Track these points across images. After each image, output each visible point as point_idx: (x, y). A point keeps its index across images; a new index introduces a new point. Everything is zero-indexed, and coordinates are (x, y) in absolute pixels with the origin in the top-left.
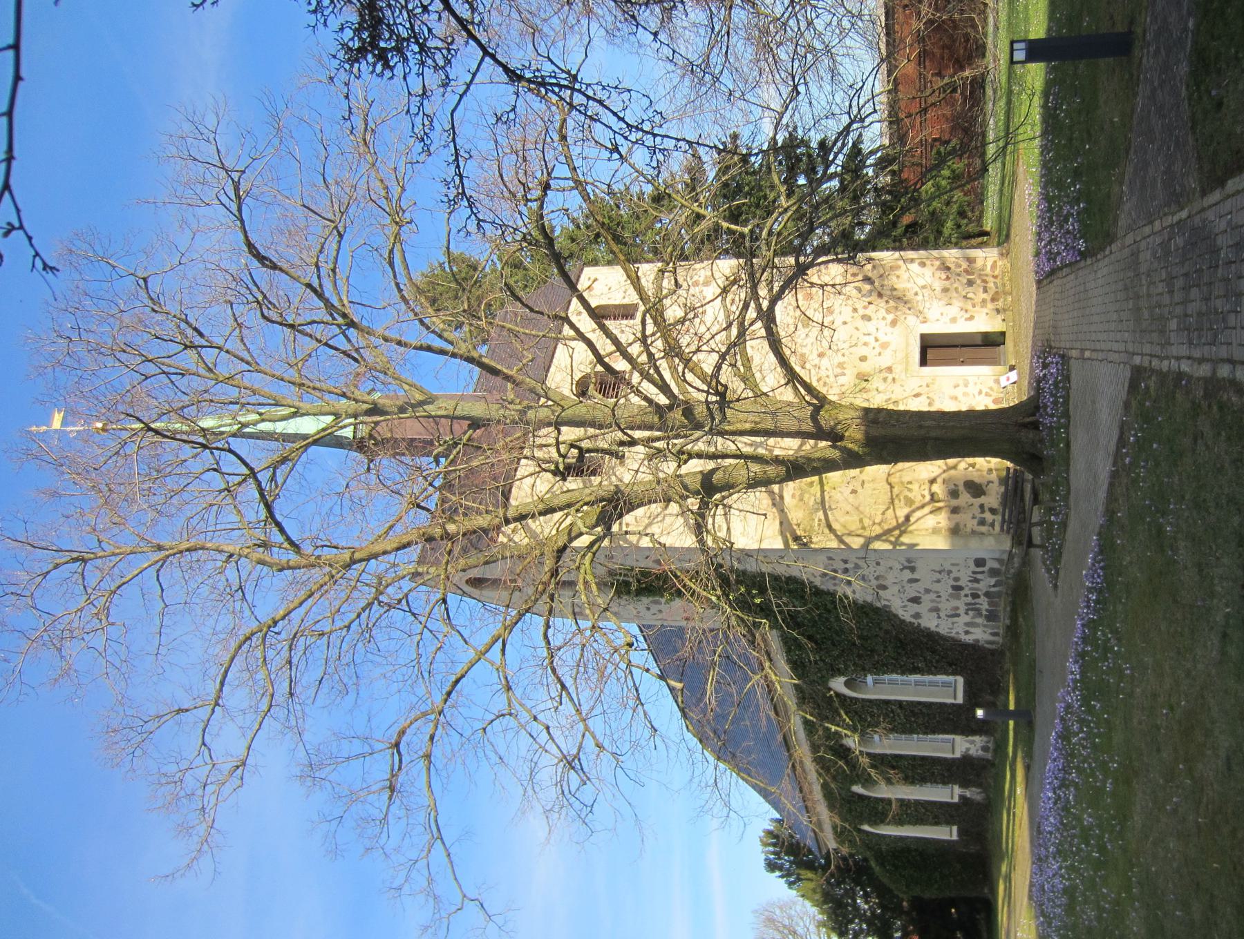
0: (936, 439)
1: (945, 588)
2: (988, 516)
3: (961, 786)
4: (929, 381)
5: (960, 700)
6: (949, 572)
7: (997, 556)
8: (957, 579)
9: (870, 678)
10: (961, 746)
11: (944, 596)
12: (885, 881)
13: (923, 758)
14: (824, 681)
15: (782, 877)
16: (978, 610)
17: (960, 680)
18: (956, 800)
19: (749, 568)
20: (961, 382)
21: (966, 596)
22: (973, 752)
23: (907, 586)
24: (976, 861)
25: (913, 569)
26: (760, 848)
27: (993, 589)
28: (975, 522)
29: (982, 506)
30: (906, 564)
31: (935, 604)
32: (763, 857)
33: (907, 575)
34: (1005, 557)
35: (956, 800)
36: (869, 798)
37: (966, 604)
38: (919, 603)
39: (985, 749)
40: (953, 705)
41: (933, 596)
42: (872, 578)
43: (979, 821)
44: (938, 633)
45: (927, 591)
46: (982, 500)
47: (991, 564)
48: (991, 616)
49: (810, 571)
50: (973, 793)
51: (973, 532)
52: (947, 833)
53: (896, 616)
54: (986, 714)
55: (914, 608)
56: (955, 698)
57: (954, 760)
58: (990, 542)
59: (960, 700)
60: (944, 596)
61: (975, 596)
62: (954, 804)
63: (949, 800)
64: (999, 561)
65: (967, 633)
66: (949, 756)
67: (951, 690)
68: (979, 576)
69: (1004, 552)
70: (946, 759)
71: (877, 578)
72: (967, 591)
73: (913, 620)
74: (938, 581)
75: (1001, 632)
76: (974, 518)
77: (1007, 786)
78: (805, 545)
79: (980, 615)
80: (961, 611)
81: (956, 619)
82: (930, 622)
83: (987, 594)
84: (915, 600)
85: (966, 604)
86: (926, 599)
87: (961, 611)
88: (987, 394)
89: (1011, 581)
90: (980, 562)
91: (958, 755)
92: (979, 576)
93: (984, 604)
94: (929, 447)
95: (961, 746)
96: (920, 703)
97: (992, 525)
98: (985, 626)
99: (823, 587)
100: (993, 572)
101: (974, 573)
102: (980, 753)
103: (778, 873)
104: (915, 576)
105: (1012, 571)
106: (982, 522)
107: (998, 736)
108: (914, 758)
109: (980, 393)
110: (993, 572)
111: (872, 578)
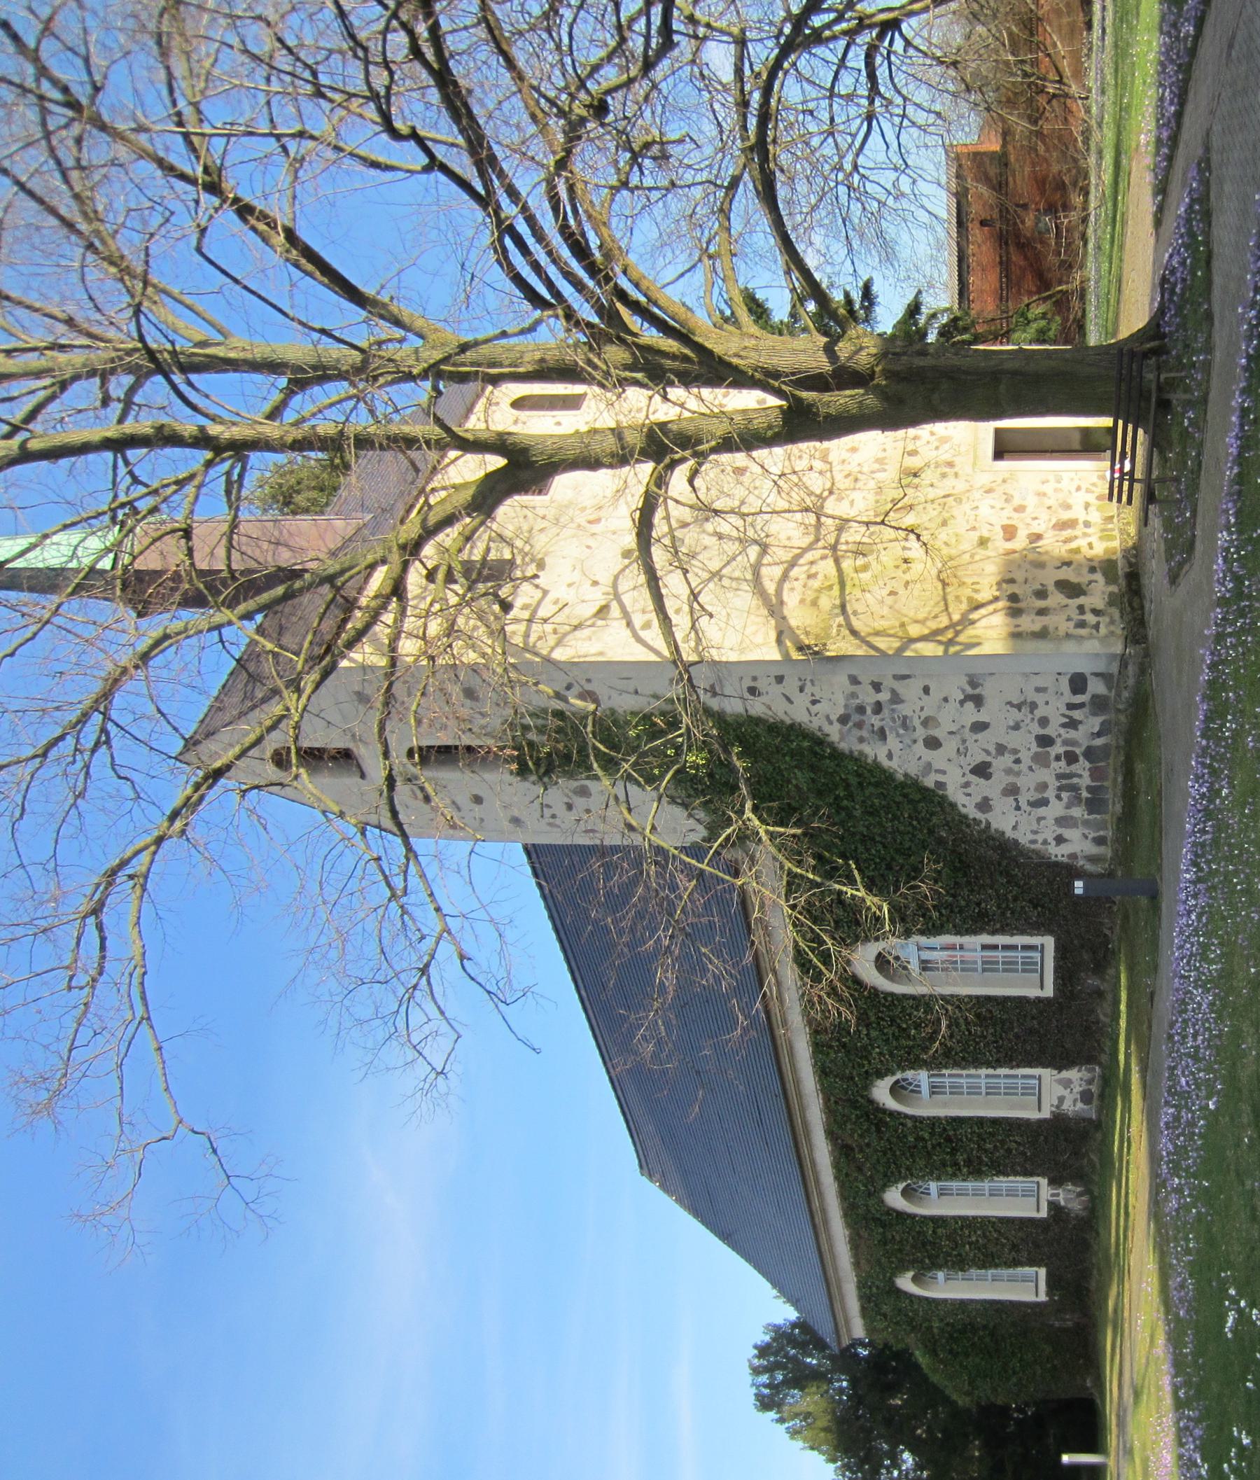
0: (1015, 373)
1: (1025, 743)
2: (1090, 618)
3: (1054, 1182)
4: (1007, 475)
5: (1049, 992)
6: (1033, 706)
7: (1101, 667)
8: (1044, 722)
9: (933, 1186)
10: (1050, 1092)
11: (1026, 757)
12: (935, 1378)
13: (995, 1122)
14: (876, 1193)
15: (781, 1420)
16: (1074, 788)
17: (1049, 942)
18: (1044, 1214)
19: (728, 710)
20: (1051, 478)
21: (1058, 758)
22: (1068, 1107)
23: (972, 738)
24: (1073, 1329)
25: (978, 701)
26: (748, 1378)
27: (1099, 742)
28: (1071, 624)
29: (1081, 609)
30: (969, 690)
31: (1011, 779)
32: (754, 1390)
33: (970, 714)
34: (1114, 668)
35: (1044, 1214)
36: (912, 1217)
37: (1059, 777)
38: (987, 776)
39: (1086, 1097)
40: (1039, 1000)
41: (1007, 759)
42: (917, 722)
43: (1074, 1252)
44: (1016, 842)
45: (1001, 749)
46: (1082, 600)
47: (1096, 687)
48: (1095, 804)
49: (819, 710)
50: (1069, 1196)
51: (1068, 636)
52: (1025, 1286)
53: (953, 806)
54: (1085, 888)
55: (981, 787)
56: (1042, 987)
57: (1041, 1122)
58: (1093, 646)
59: (1049, 992)
60: (1026, 757)
61: (1071, 758)
62: (1041, 1220)
63: (1034, 1214)
64: (1104, 676)
65: (1060, 840)
66: (1033, 1115)
67: (1037, 975)
68: (1077, 714)
69: (1114, 656)
70: (1027, 1122)
71: (926, 723)
72: (1058, 749)
73: (979, 816)
74: (1016, 727)
75: (1109, 834)
76: (1069, 619)
77: (1111, 1303)
78: (816, 653)
79: (1078, 799)
80: (1050, 794)
81: (1042, 811)
82: (1003, 819)
83: (1090, 753)
84: (982, 770)
85: (1059, 777)
86: (1000, 764)
87: (1050, 794)
88: (1088, 491)
89: (1122, 718)
90: (1078, 683)
91: (1046, 1114)
92: (1077, 714)
93: (1083, 773)
94: (1002, 388)
95: (1050, 1092)
96: (989, 999)
97: (1097, 627)
98: (1086, 823)
99: (844, 746)
100: (1099, 705)
101: (1071, 707)
102: (1080, 1105)
103: (772, 1415)
104: (983, 717)
105: (1126, 694)
106: (1082, 624)
107: (1104, 1058)
108: (981, 1121)
109: (1079, 489)
110: (1099, 705)
111: (917, 722)
